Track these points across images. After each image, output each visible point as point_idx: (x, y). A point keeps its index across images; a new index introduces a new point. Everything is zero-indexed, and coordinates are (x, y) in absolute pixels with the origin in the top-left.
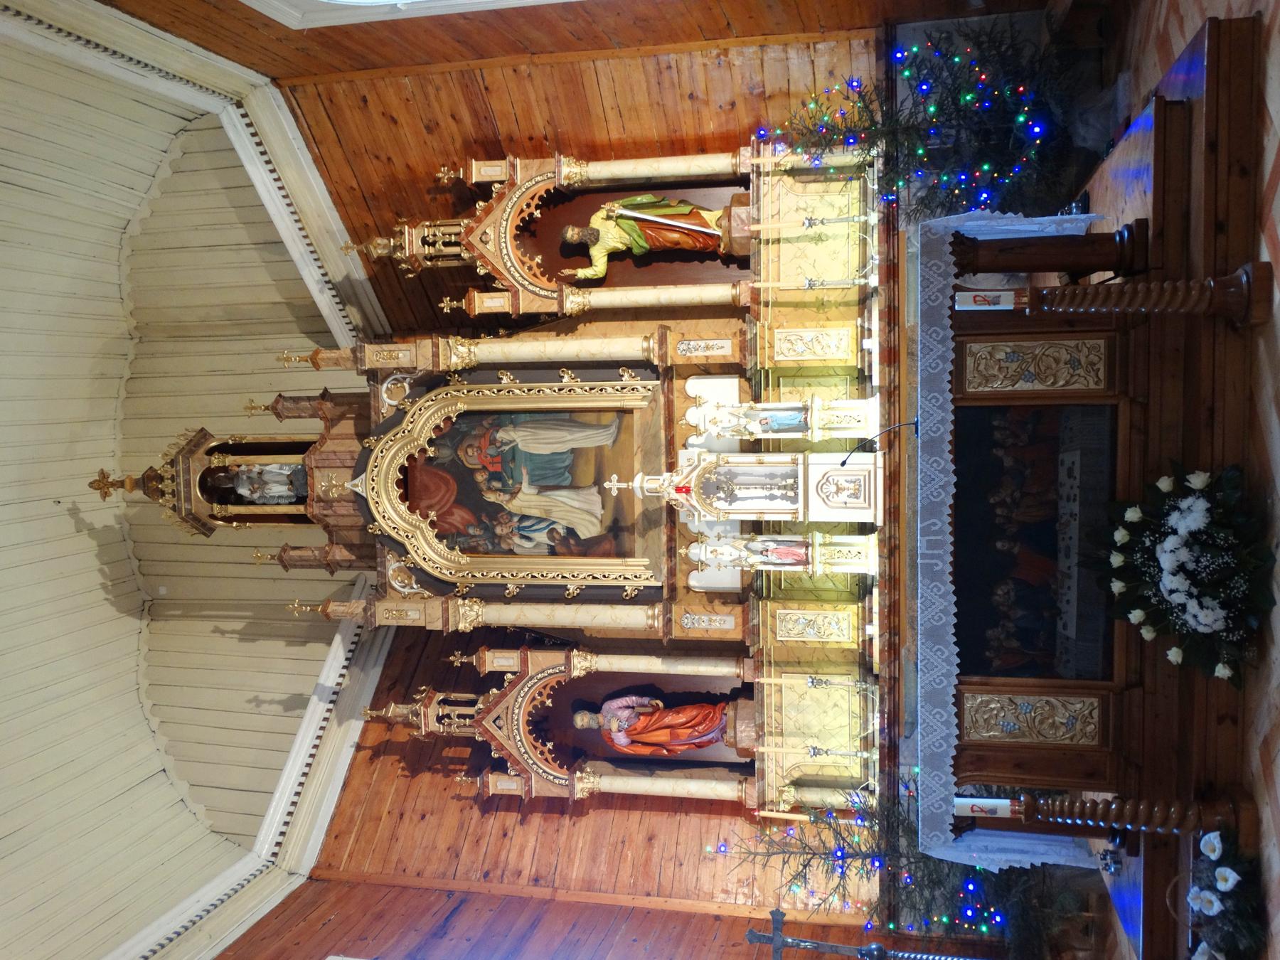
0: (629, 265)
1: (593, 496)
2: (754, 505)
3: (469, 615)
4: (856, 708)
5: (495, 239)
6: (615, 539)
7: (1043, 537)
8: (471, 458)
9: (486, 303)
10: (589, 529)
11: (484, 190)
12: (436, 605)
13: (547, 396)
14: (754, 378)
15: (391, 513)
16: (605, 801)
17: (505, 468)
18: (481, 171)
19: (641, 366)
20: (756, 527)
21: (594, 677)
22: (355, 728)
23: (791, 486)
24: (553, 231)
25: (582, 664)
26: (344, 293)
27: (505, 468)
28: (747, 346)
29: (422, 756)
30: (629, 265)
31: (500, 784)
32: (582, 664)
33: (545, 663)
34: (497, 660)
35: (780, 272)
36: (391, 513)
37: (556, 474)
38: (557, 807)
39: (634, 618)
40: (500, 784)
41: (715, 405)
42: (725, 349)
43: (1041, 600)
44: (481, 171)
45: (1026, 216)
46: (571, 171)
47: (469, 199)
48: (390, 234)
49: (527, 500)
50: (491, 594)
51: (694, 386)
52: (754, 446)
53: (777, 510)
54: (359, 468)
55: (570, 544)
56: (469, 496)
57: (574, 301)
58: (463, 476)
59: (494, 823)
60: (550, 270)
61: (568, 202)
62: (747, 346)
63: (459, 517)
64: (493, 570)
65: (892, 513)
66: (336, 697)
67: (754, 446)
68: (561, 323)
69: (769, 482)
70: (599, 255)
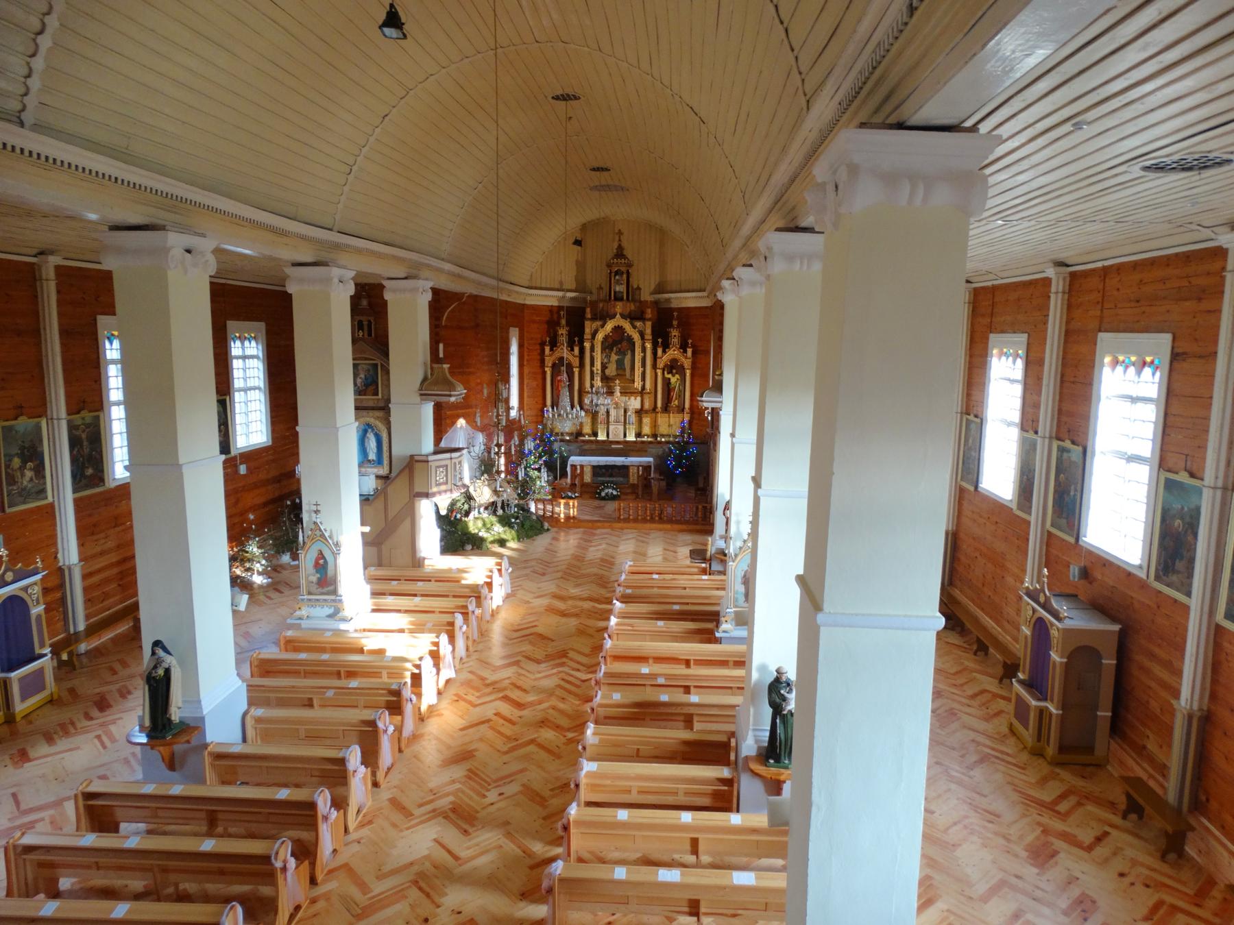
0: (667, 383)
1: (614, 373)
2: (613, 413)
3: (587, 345)
4: (540, 630)
5: (673, 353)
6: (605, 379)
7: (611, 476)
8: (625, 344)
9: (660, 351)
10: (607, 372)
11: (685, 351)
12: (589, 337)
13: (638, 364)
14: (640, 413)
15: (609, 326)
16: (544, 373)
17: (622, 353)
18: (690, 351)
19: (643, 388)
20: (608, 412)
21: (573, 373)
22: (556, 304)
23: (617, 421)
24: (673, 367)
25: (576, 371)
26: (668, 300)
27: (622, 353)
28: (646, 412)
29: (553, 324)
30: (667, 383)
31: (547, 349)
32: (576, 371)
33: (576, 362)
34: (576, 350)
35: (662, 420)
36: (609, 326)
37: (620, 364)
38: (542, 361)
39: (588, 385)
40: (547, 349)
41: (635, 403)
42: (647, 406)
43: (603, 475)
44: (690, 351)
45: (298, 462)
46: (688, 373)
47: (684, 347)
48: (678, 326)
49: (614, 357)
50: (592, 349)
51: (639, 398)
52: (625, 411)
53: (612, 419)
54: (623, 316)
55: (604, 367)
56: (615, 343)
57: (659, 372)
58: (620, 342)
59: (538, 347)
60: (666, 366)
61: (681, 371)
62: (646, 412)
63: (610, 340)
64: (598, 349)
65: (612, 442)
66: (564, 297)
67: (625, 411)
68: (654, 366)
69: (617, 416)
70: (670, 376)
